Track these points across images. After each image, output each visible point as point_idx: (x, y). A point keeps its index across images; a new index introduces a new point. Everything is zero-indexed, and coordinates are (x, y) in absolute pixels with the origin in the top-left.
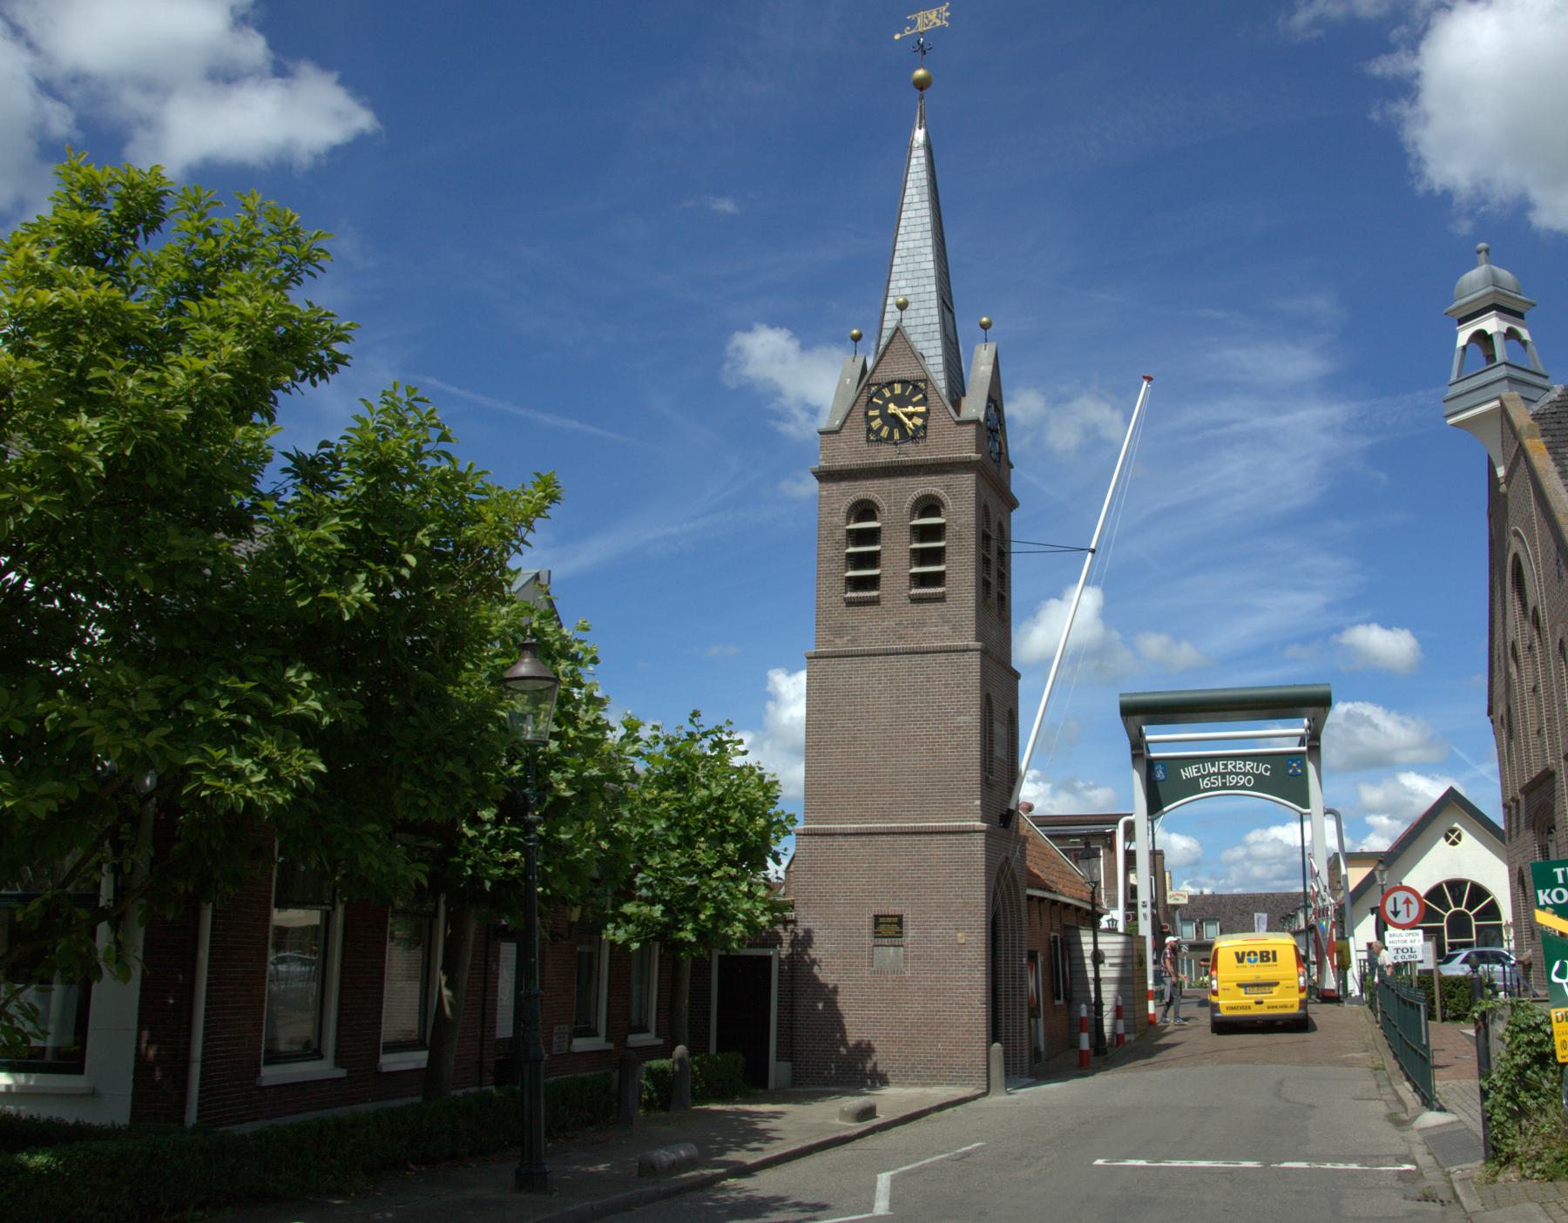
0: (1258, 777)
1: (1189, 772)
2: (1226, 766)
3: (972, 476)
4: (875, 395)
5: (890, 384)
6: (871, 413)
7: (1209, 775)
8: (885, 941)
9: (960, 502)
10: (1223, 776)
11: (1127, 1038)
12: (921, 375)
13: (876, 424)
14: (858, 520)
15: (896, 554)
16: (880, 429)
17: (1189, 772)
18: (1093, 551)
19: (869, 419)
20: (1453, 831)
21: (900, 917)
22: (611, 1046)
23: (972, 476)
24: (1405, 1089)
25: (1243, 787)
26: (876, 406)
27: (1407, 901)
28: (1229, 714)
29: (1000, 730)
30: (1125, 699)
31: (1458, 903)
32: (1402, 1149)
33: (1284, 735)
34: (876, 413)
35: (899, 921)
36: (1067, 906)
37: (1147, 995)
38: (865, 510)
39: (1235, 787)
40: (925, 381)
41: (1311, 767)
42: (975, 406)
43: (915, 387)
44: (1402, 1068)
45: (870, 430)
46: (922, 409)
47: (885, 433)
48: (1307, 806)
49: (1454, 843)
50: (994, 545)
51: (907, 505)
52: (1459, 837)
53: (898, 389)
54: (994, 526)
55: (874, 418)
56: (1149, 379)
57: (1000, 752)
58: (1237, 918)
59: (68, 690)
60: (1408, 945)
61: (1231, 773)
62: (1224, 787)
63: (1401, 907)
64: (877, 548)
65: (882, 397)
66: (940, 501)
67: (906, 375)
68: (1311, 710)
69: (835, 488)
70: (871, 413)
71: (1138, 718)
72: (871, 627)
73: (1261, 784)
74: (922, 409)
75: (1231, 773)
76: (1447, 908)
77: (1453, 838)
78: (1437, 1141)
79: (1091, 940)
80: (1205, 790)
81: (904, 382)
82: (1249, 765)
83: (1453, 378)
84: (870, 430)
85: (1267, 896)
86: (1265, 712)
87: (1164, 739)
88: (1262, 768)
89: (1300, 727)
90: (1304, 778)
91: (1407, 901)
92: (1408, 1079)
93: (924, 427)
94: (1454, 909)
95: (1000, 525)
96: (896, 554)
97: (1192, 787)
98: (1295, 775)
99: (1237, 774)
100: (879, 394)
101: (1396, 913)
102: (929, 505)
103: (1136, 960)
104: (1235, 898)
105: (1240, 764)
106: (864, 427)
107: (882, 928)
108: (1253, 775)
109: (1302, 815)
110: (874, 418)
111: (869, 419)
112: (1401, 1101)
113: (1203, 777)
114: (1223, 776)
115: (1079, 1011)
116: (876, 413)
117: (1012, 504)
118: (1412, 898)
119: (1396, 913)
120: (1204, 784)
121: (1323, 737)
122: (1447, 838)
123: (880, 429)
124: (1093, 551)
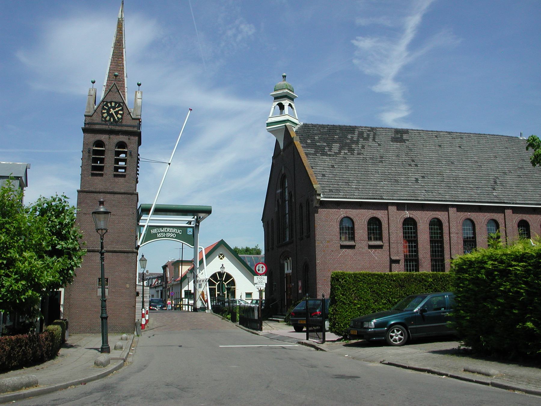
4: (105, 105)
6: (103, 111)
7: (161, 232)
10: (166, 233)
12: (121, 101)
13: (105, 115)
14: (118, 148)
16: (106, 117)
18: (169, 164)
22: (324, 290)
25: (172, 237)
26: (105, 109)
28: (171, 213)
33: (182, 221)
34: (106, 111)
37: (225, 302)
38: (99, 143)
39: (169, 237)
45: (103, 117)
49: (221, 259)
51: (115, 145)
53: (113, 104)
55: (105, 113)
59: (197, 219)
62: (166, 237)
66: (126, 144)
67: (116, 100)
69: (89, 135)
70: (103, 111)
72: (99, 183)
73: (178, 237)
77: (221, 256)
80: (159, 238)
81: (116, 103)
83: (270, 116)
86: (174, 213)
88: (179, 231)
89: (190, 218)
102: (122, 145)
105: (171, 229)
108: (176, 233)
110: (105, 113)
113: (159, 233)
114: (166, 233)
116: (106, 111)
119: (259, 270)
120: (158, 235)
122: (219, 257)
123: (106, 117)
124: (169, 164)
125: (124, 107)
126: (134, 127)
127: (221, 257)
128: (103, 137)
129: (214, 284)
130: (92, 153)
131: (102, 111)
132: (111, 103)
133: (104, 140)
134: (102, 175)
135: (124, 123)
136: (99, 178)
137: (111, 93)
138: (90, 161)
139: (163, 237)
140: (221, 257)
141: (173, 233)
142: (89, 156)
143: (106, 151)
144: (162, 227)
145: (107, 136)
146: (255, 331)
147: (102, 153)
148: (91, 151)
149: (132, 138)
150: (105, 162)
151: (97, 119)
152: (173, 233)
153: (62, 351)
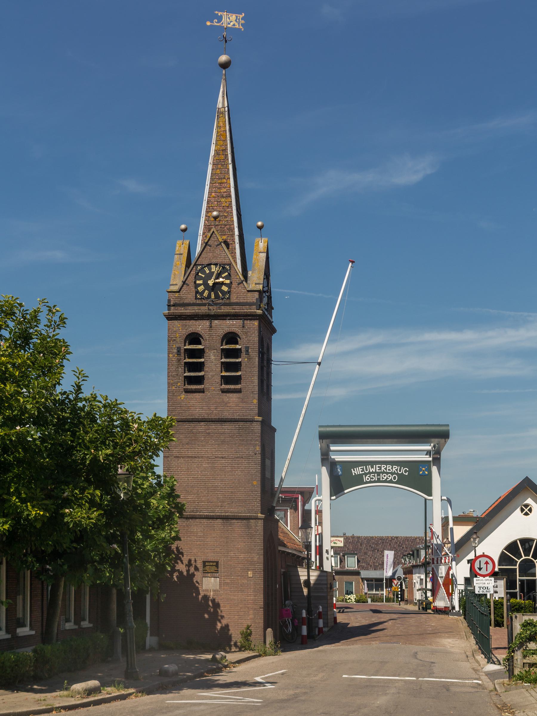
0: (401, 476)
1: (357, 471)
2: (380, 468)
3: (256, 323)
5: (209, 265)
6: (198, 282)
7: (370, 473)
8: (209, 575)
9: (249, 334)
10: (379, 474)
11: (324, 629)
13: (201, 288)
14: (190, 344)
15: (213, 362)
16: (203, 292)
17: (357, 471)
18: (319, 364)
19: (197, 286)
20: (526, 506)
21: (217, 563)
23: (256, 323)
24: (480, 657)
25: (391, 481)
26: (201, 278)
27: (487, 563)
29: (268, 462)
30: (322, 429)
31: (527, 553)
32: (477, 676)
33: (418, 453)
34: (201, 282)
35: (217, 564)
36: (289, 553)
38: (194, 338)
40: (230, 265)
41: (434, 469)
42: (256, 278)
43: (223, 268)
44: (480, 648)
45: (197, 292)
46: (228, 282)
47: (206, 294)
48: (430, 495)
49: (526, 514)
50: (265, 357)
51: (219, 339)
52: (530, 510)
54: (265, 349)
56: (353, 262)
57: (268, 475)
58: (370, 553)
60: (486, 585)
61: (384, 472)
62: (379, 481)
63: (483, 566)
64: (202, 360)
65: (204, 272)
67: (219, 261)
68: (436, 440)
69: (177, 324)
70: (198, 282)
71: (328, 441)
72: (196, 405)
73: (402, 480)
74: (228, 282)
75: (384, 472)
76: (515, 563)
78: (492, 675)
79: (306, 574)
82: (395, 468)
84: (197, 292)
85: (392, 538)
87: (342, 453)
88: (403, 470)
90: (429, 478)
91: (487, 563)
92: (483, 653)
93: (229, 292)
94: (524, 558)
95: (268, 344)
96: (213, 362)
97: (359, 480)
98: (424, 475)
99: (387, 473)
100: (202, 270)
101: (480, 569)
102: (231, 338)
103: (329, 586)
104: (369, 540)
105: (389, 467)
106: (194, 289)
107: (207, 568)
108: (397, 474)
109: (426, 500)
111: (197, 286)
112: (477, 662)
113: (366, 474)
114: (379, 474)
115: (301, 614)
117: (273, 331)
118: (489, 561)
119: (480, 569)
120: (366, 478)
121: (442, 453)
122: (522, 510)
123: (203, 292)
124: (319, 364)
125: (232, 272)
126: (250, 304)
127: (526, 510)
128: (200, 327)
129: (514, 563)
130: (183, 355)
131: (195, 282)
132: (209, 265)
133: (202, 333)
134: (202, 391)
135: (234, 299)
136: (197, 395)
137: (208, 247)
138: (181, 370)
139: (375, 482)
140: (526, 510)
141: (392, 474)
142: (179, 360)
143: (207, 351)
144: (372, 463)
145: (207, 323)
146: (220, 674)
147: (200, 353)
148: (182, 351)
149: (247, 322)
150: (206, 369)
151: (189, 296)
152: (392, 474)
153: (486, 660)
